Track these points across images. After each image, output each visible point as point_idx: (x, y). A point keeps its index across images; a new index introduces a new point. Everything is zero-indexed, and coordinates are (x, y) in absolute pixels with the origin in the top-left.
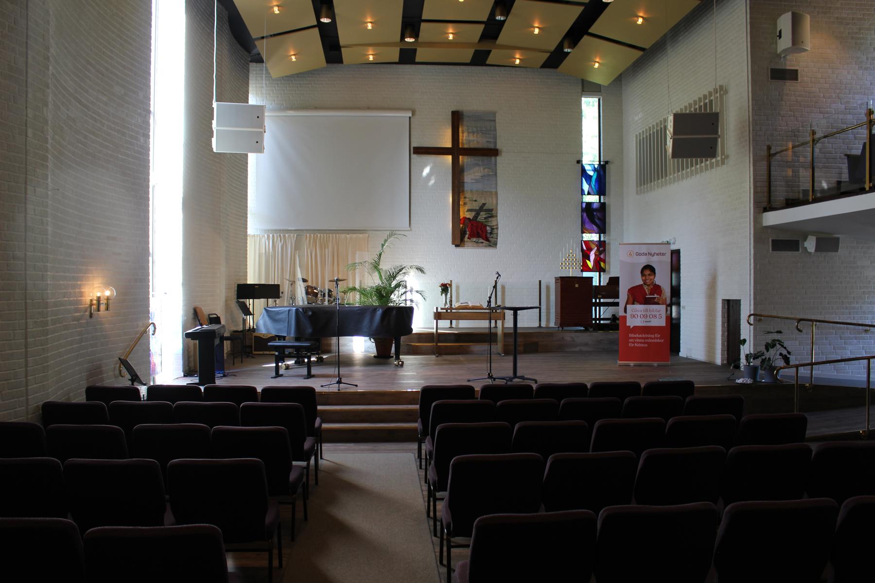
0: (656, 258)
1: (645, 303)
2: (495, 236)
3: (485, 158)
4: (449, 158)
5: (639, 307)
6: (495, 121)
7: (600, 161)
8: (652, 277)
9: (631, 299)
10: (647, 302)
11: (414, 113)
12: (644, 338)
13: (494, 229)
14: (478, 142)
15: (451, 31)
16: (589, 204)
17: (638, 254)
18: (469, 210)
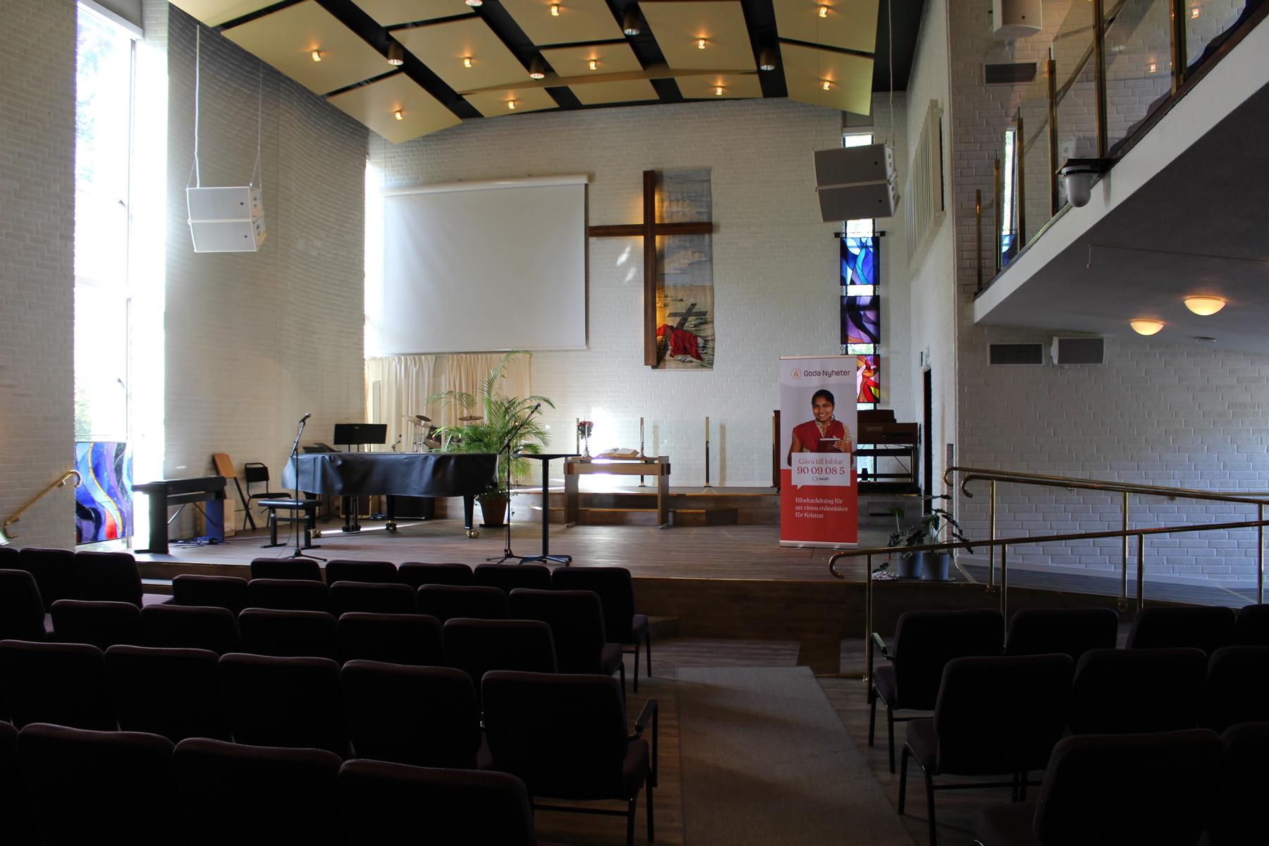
0: (834, 379)
1: (818, 451)
2: (709, 351)
3: (695, 237)
4: (641, 239)
6: (709, 181)
8: (829, 409)
9: (798, 444)
10: (822, 447)
11: (591, 178)
12: (818, 505)
14: (684, 214)
15: (593, 57)
17: (808, 374)
18: (673, 315)
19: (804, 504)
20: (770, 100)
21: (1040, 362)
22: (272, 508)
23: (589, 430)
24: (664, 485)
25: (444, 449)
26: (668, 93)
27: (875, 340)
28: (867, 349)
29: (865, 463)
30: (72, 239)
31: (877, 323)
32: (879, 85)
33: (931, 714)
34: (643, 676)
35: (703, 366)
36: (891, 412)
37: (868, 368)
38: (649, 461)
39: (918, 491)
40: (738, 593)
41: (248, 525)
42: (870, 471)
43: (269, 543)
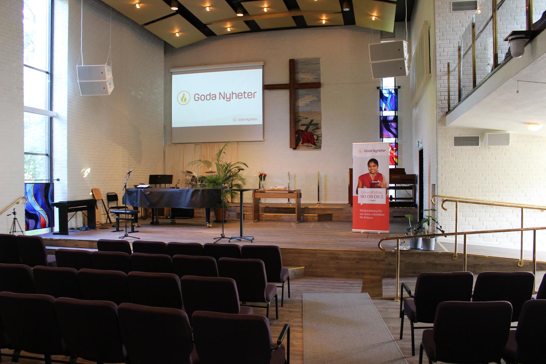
1: (371, 187)
5: (367, 190)
7: (395, 87)
8: (376, 168)
9: (361, 184)
10: (372, 186)
13: (319, 137)
16: (386, 117)
17: (366, 151)
19: (364, 213)
20: (348, 26)
21: (478, 145)
22: (118, 214)
23: (264, 178)
24: (299, 203)
25: (199, 186)
26: (301, 23)
27: (396, 136)
28: (392, 140)
29: (392, 193)
30: (22, 89)
31: (396, 129)
32: (399, 19)
33: (432, 325)
34: (286, 297)
35: (316, 148)
36: (403, 169)
37: (392, 149)
38: (290, 192)
39: (416, 206)
40: (333, 256)
41: (108, 221)
42: (394, 197)
43: (115, 230)
